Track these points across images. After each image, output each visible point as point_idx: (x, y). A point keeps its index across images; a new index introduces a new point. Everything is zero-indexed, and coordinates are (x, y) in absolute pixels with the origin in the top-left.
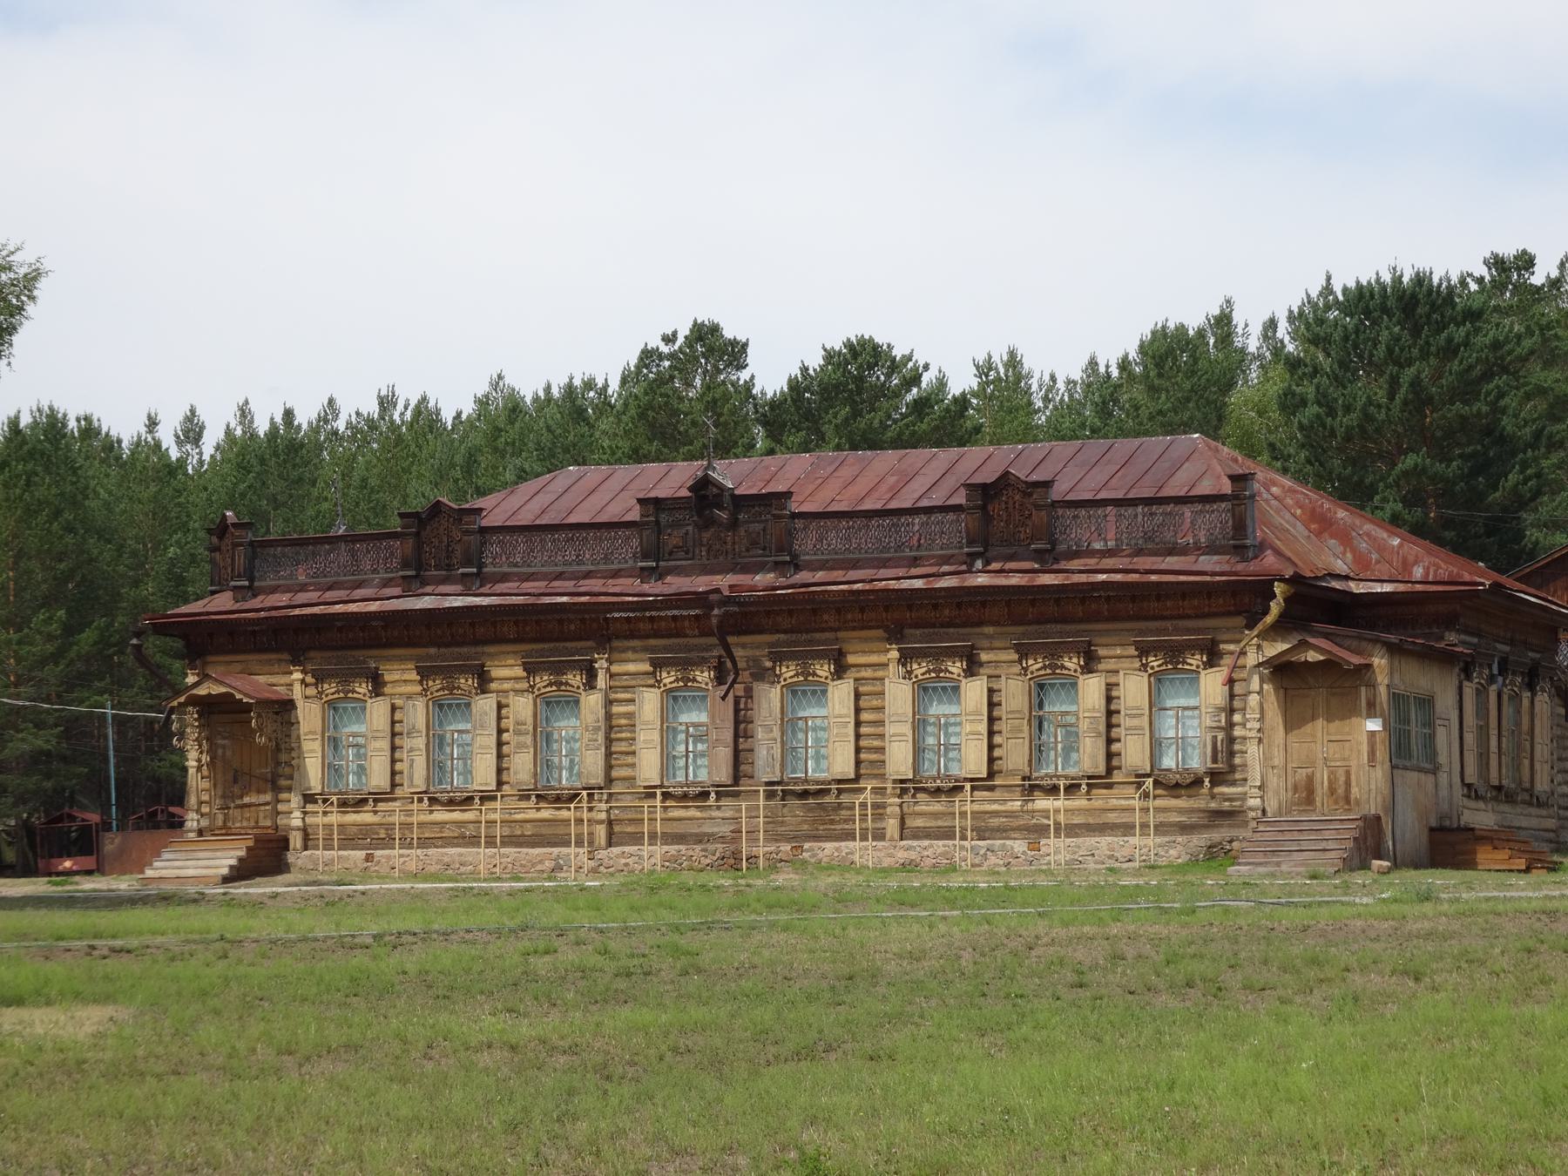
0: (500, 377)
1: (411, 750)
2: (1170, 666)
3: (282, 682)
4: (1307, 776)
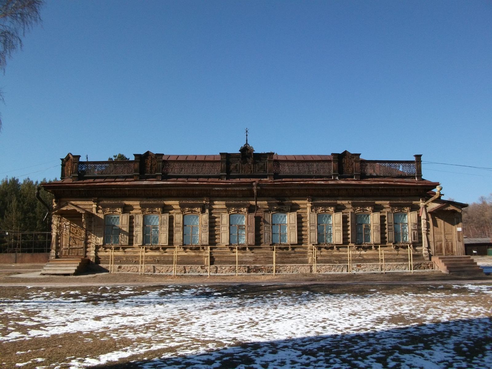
0: (45, 179)
1: (137, 231)
3: (89, 208)
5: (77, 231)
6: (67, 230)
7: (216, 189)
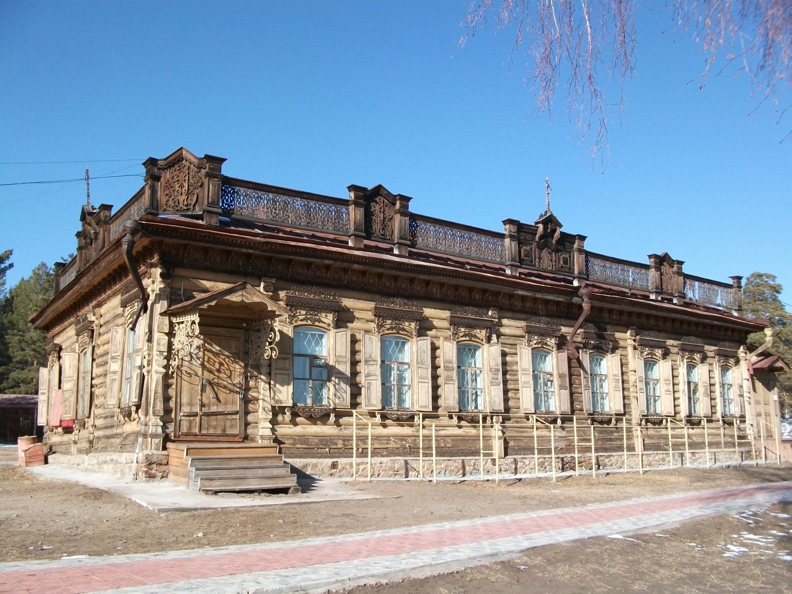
1: (368, 375)
5: (221, 364)
6: (194, 362)
7: (521, 292)
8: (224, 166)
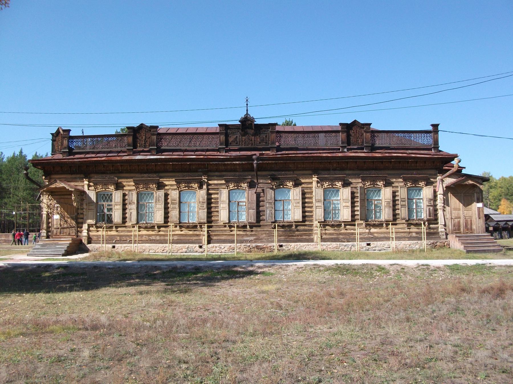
2: (414, 185)
4: (458, 222)
8: (371, 126)
